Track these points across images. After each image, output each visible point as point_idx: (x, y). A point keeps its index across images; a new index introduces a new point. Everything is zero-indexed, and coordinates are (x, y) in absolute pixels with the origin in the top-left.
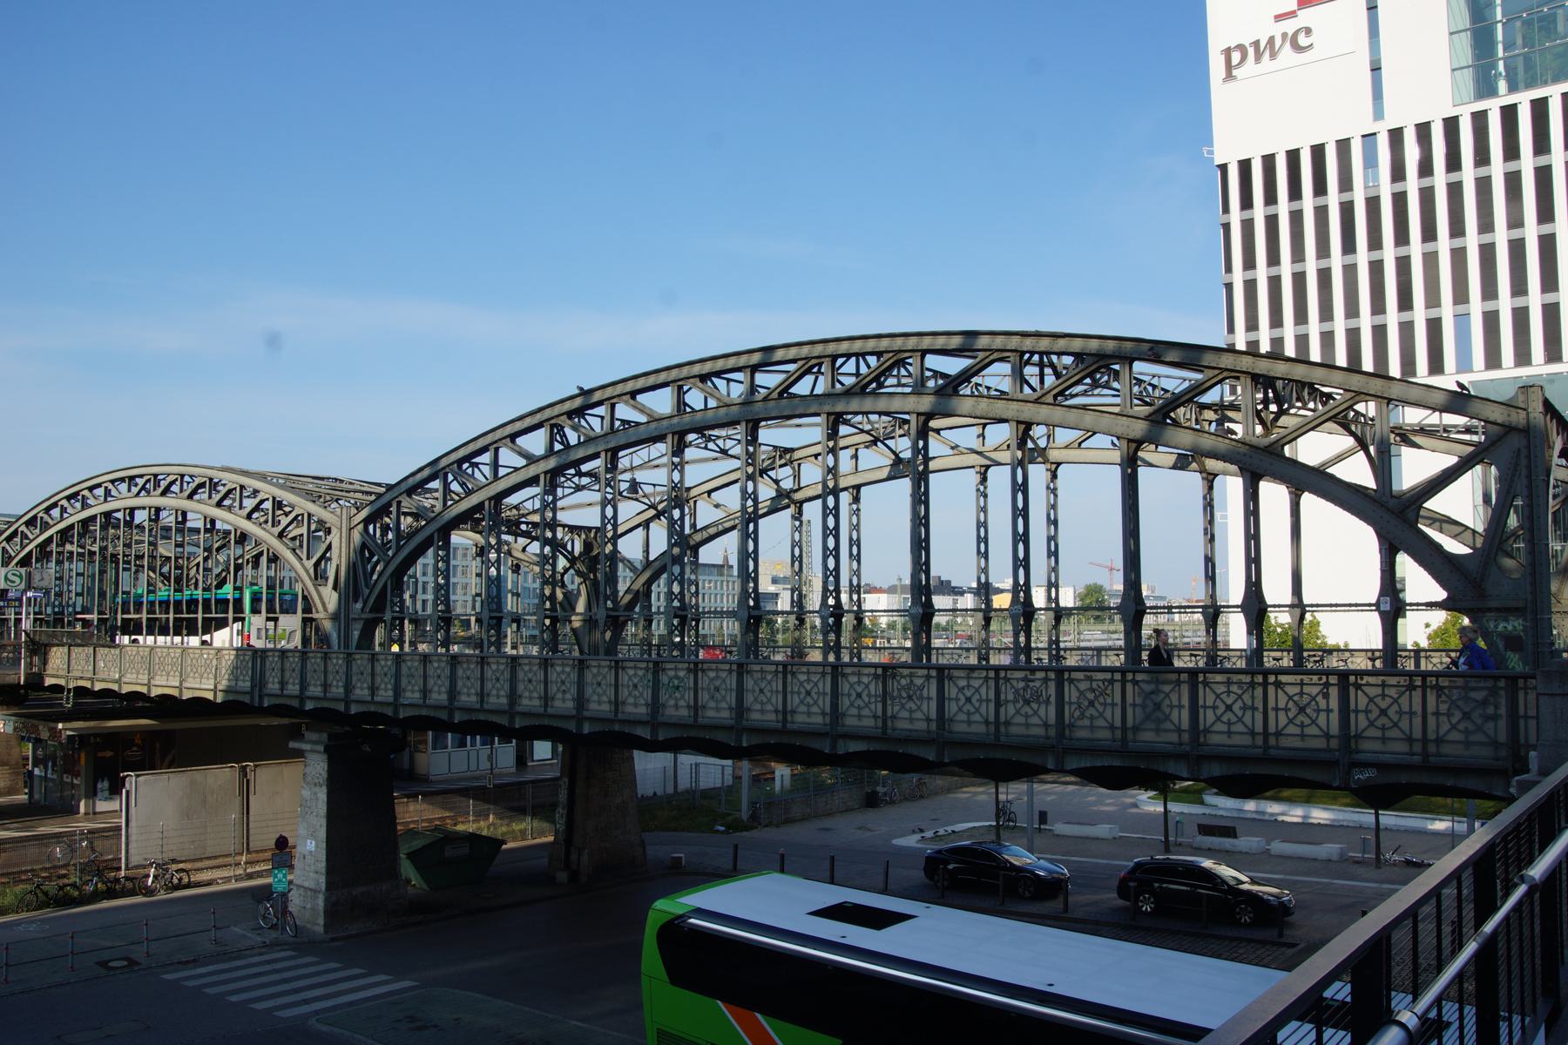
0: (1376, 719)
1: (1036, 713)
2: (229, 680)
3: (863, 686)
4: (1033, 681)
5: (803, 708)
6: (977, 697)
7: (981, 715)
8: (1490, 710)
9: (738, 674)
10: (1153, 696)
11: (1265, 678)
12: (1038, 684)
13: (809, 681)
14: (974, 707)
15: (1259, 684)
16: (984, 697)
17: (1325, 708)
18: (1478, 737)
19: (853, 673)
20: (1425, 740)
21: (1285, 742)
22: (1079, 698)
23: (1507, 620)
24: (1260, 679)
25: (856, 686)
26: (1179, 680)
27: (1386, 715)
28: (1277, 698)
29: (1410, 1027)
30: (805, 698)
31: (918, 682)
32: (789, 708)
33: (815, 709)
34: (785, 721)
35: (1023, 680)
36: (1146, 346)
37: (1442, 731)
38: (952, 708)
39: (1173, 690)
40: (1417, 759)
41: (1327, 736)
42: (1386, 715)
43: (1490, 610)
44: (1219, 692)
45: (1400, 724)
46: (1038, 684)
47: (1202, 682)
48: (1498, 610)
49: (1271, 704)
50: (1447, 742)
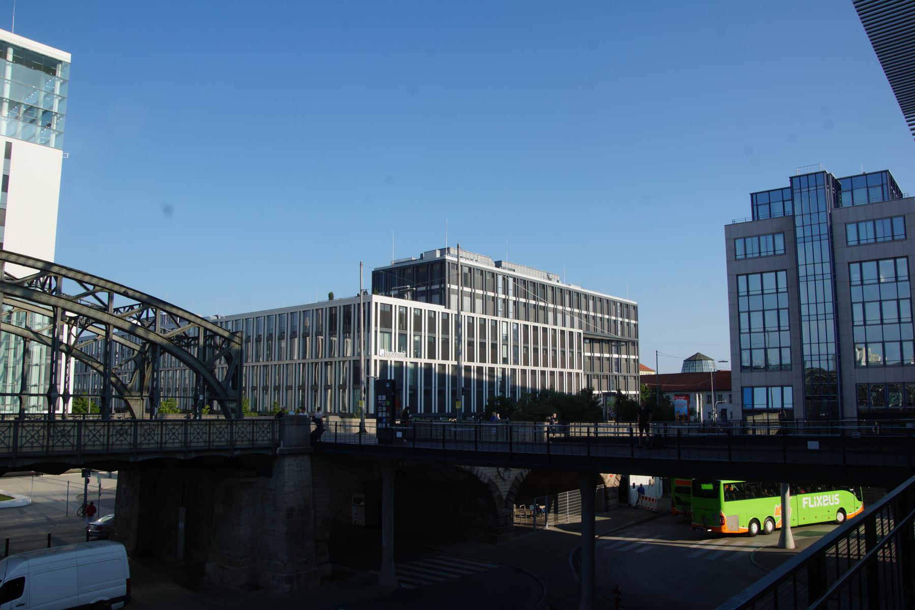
0: (29, 440)
1: (126, 439)
2: (729, 421)
3: (244, 429)
4: (124, 426)
5: (170, 441)
6: (195, 435)
7: (247, 438)
8: (269, 430)
9: (134, 426)
10: (172, 430)
11: (109, 424)
12: (126, 428)
13: (243, 427)
14: (29, 440)
15: (22, 424)
16: (237, 434)
17: (8, 435)
18: (97, 443)
19: (147, 425)
20: (108, 444)
21: (115, 447)
22: (238, 430)
23: (232, 404)
24: (106, 424)
26: (44, 425)
27: (173, 435)
28: (213, 430)
29: (847, 518)
30: (241, 434)
31: (68, 429)
32: (255, 439)
33: (245, 439)
34: (253, 444)
35: (120, 426)
36: (345, 325)
37: (23, 443)
38: (235, 436)
39: (180, 428)
40: (207, 447)
41: (73, 445)
42: (173, 435)
43: (228, 400)
44: (5, 432)
45: (70, 440)
46: (126, 428)
47: (212, 424)
48: (231, 400)
49: (212, 431)
50: (56, 446)
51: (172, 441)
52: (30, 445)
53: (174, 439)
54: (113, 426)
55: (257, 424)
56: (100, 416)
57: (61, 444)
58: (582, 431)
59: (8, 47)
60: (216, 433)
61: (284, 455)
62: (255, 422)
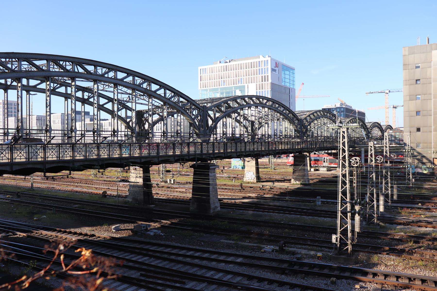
3: (3, 150)
16: (32, 153)
25: (53, 154)
34: (149, 155)
49: (30, 151)
51: (51, 156)
52: (19, 158)
53: (20, 156)
54: (112, 145)
55: (84, 146)
56: (231, 135)
57: (19, 158)
58: (9, 128)
59: (160, 87)
60: (33, 152)
61: (244, 163)
62: (61, 145)
